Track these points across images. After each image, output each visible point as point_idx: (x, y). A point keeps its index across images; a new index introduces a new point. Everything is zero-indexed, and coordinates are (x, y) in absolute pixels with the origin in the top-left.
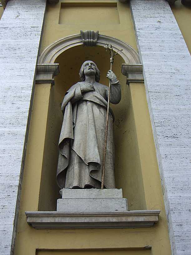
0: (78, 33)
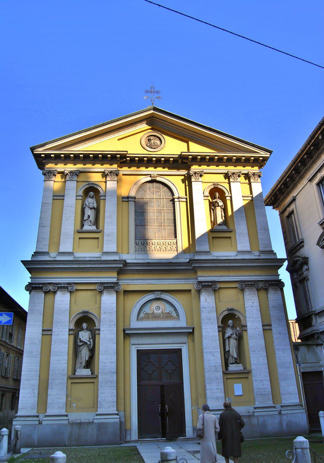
0: (226, 309)
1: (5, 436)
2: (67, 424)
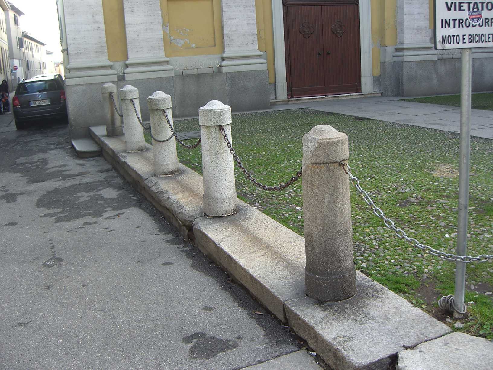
1: (227, 127)
2: (173, 77)
